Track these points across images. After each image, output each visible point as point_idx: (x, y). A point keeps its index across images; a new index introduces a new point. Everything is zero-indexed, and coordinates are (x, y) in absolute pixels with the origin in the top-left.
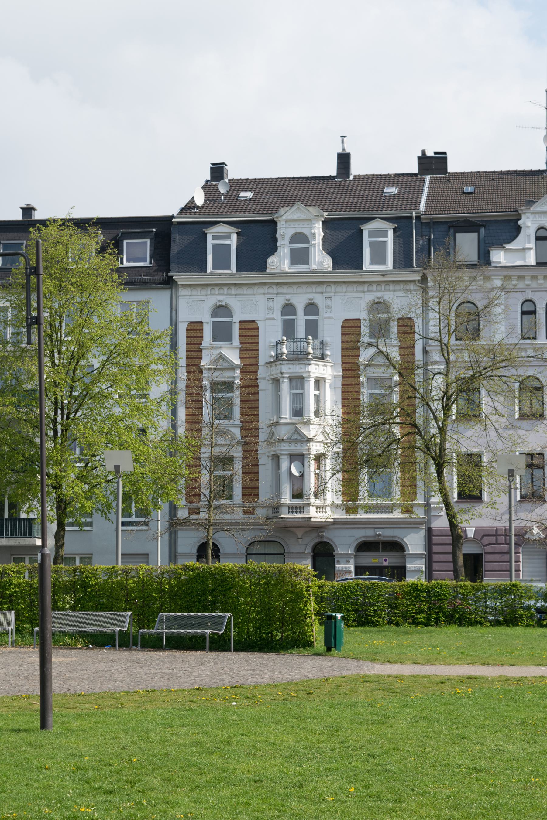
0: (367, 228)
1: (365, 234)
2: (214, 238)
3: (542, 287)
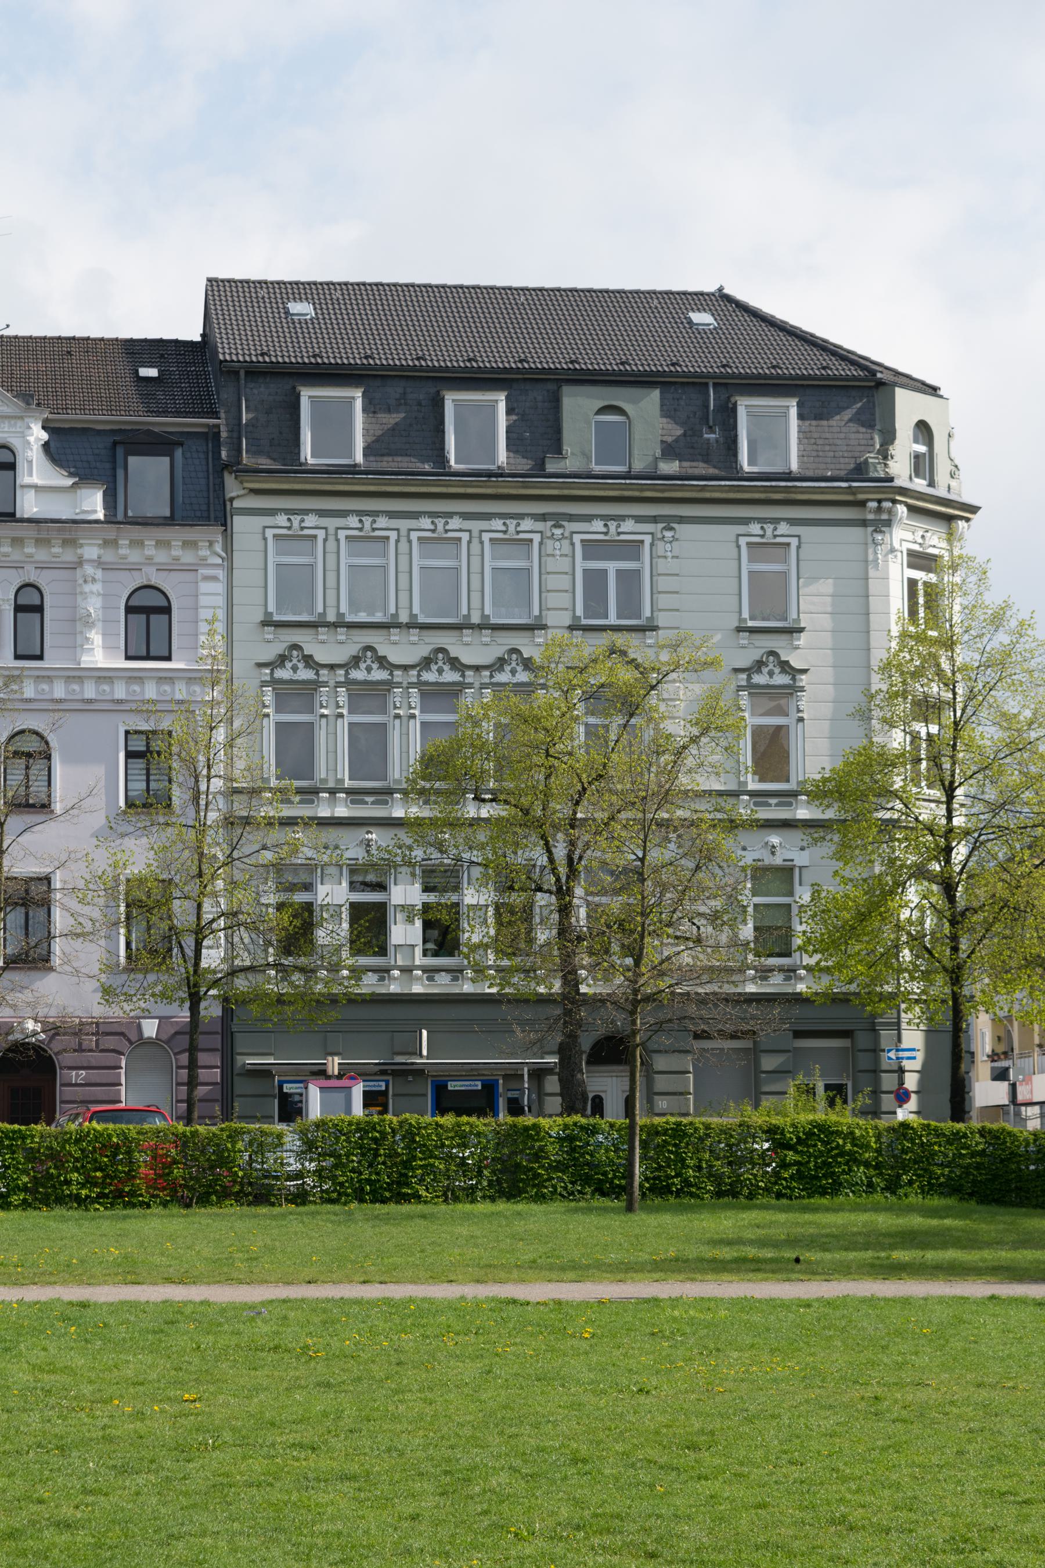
3: (58, 560)
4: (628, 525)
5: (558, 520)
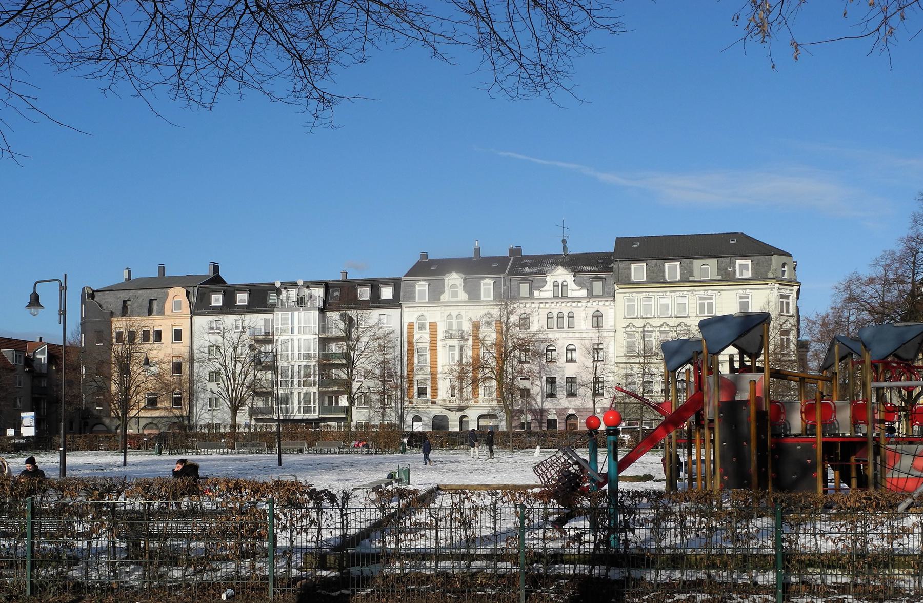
0: (482, 283)
1: (482, 284)
2: (418, 287)
4: (709, 292)
5: (692, 291)
